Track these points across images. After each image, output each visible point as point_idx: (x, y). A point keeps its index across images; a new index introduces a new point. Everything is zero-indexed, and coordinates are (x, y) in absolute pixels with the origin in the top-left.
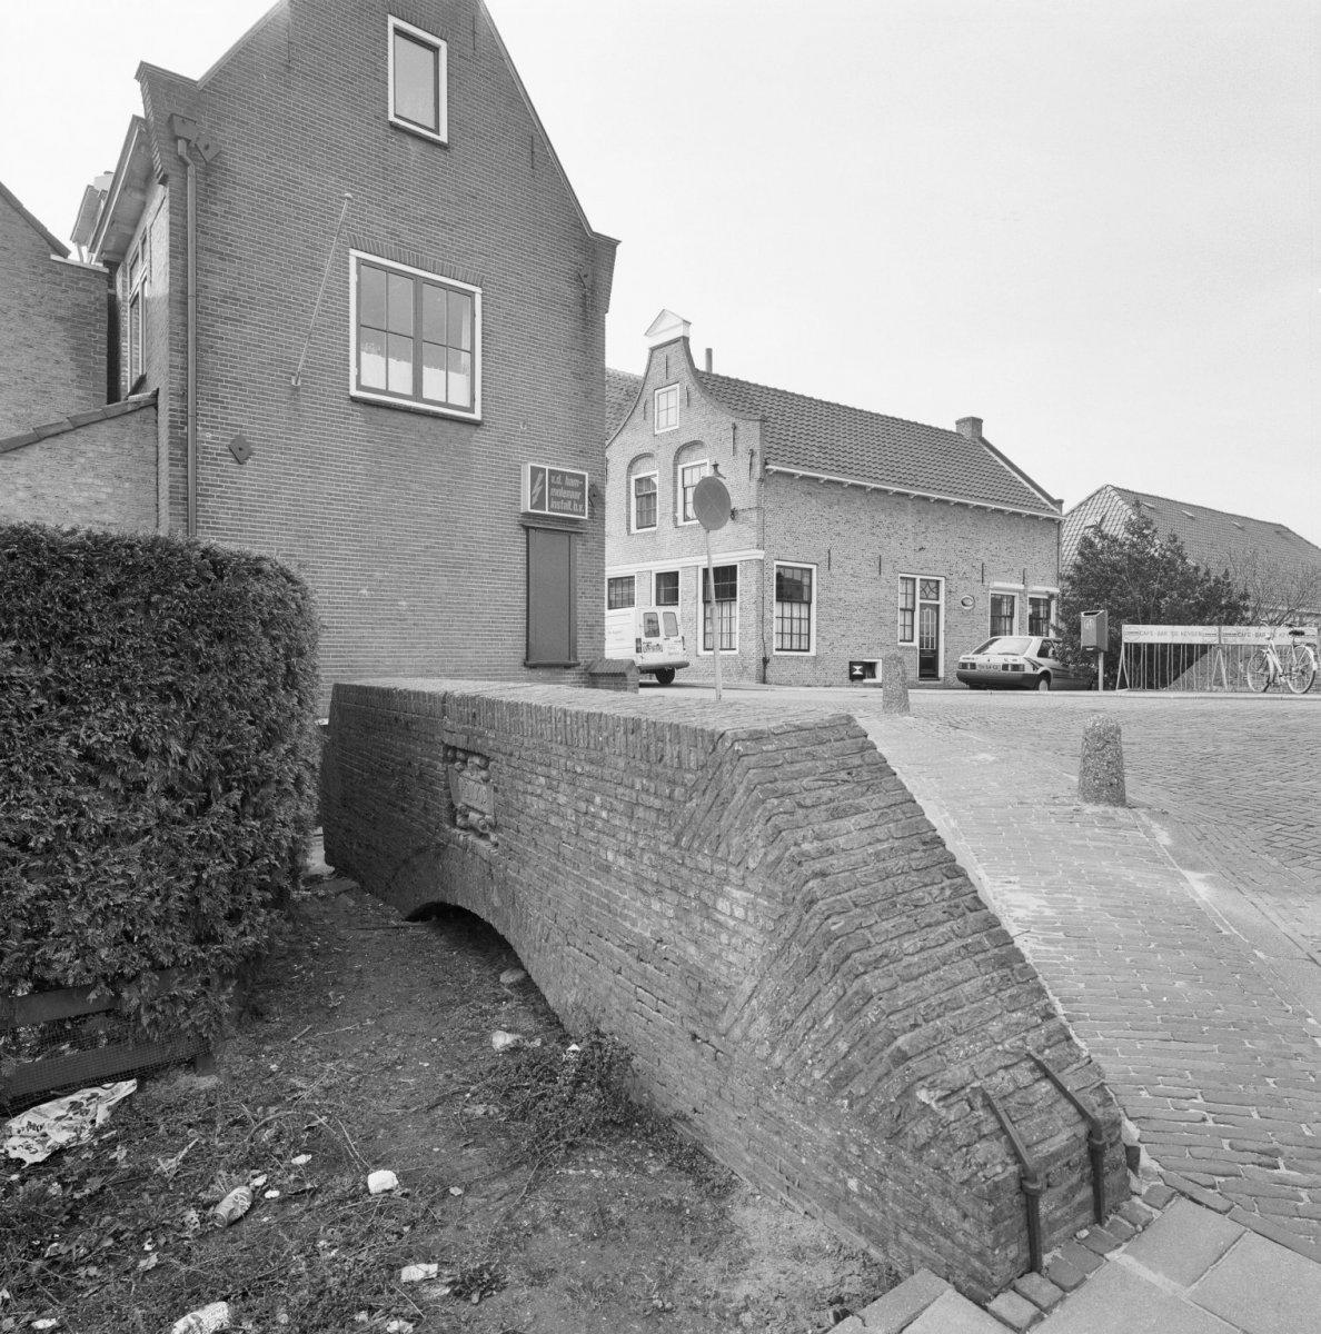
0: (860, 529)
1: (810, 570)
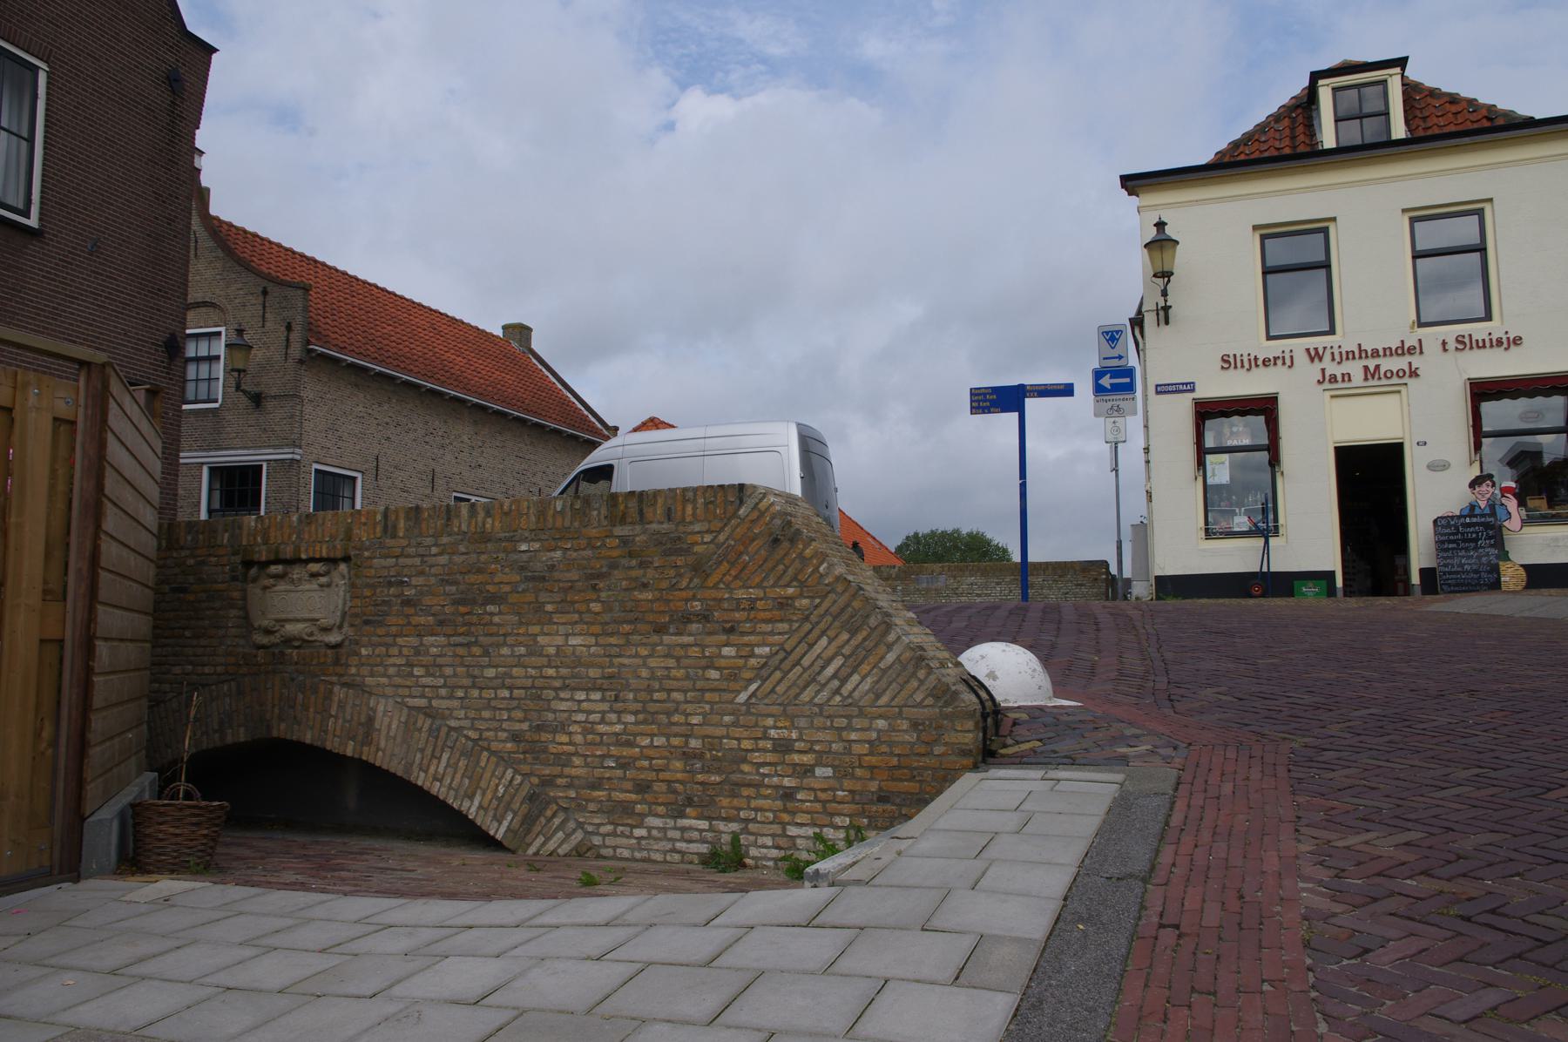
0: (412, 435)
1: (354, 479)
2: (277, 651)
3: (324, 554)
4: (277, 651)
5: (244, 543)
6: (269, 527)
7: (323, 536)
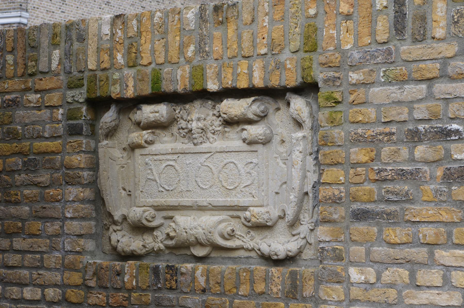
2: (162, 265)
3: (258, 82)
4: (162, 265)
5: (92, 65)
6: (140, 33)
7: (254, 45)
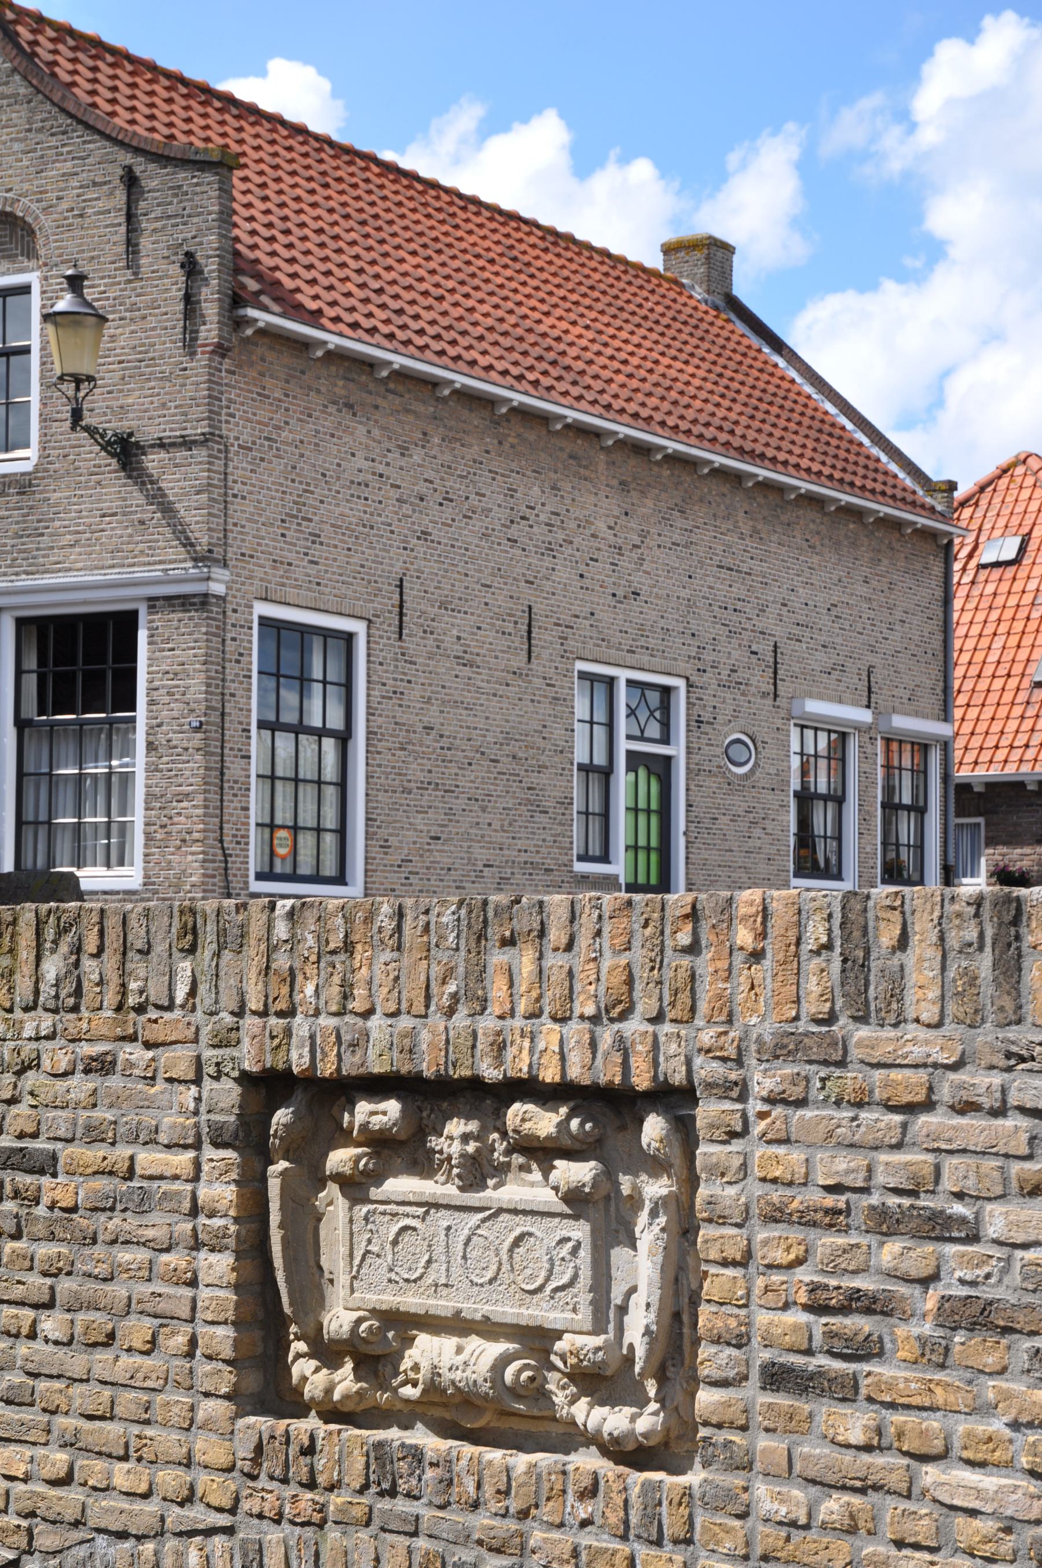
0: (477, 524)
1: (349, 638)
